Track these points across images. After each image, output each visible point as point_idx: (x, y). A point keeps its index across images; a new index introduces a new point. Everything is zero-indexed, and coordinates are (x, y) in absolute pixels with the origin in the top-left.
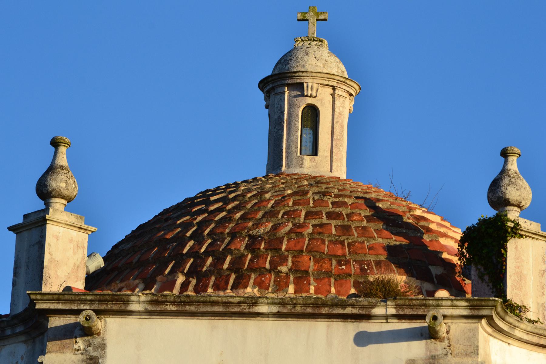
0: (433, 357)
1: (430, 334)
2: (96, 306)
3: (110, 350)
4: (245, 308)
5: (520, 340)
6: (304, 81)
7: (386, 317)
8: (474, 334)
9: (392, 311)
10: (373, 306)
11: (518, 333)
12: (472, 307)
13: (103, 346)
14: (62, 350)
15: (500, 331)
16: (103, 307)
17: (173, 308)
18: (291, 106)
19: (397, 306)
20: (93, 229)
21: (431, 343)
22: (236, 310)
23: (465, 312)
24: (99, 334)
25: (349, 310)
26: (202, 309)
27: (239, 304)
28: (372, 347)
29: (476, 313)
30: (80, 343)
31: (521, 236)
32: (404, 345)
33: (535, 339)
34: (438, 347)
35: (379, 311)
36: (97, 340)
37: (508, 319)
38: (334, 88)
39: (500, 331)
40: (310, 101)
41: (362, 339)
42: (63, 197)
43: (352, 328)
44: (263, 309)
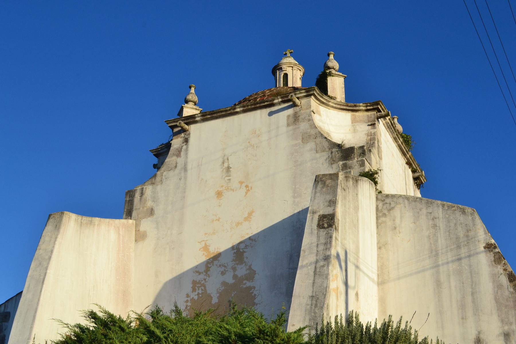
0: (296, 112)
1: (295, 105)
2: (186, 121)
3: (191, 135)
4: (232, 111)
5: (333, 107)
6: (282, 66)
7: (279, 103)
8: (310, 102)
9: (280, 100)
10: (274, 100)
11: (331, 104)
12: (307, 92)
13: (189, 134)
14: (177, 138)
15: (323, 103)
16: (188, 121)
17: (209, 116)
18: (279, 75)
19: (282, 98)
20: (201, 109)
21: (295, 108)
22: (229, 112)
23: (305, 94)
24: (188, 130)
25: (266, 103)
26: (219, 114)
27: (230, 110)
28: (274, 116)
29: (309, 93)
30: (183, 135)
31: (333, 76)
32: (286, 111)
33: (339, 106)
34: (297, 109)
35: (276, 101)
36: (188, 133)
37: (324, 97)
38: (292, 67)
39: (323, 103)
40: (284, 72)
41: (271, 114)
42: (192, 102)
43: (268, 110)
44: (238, 110)
